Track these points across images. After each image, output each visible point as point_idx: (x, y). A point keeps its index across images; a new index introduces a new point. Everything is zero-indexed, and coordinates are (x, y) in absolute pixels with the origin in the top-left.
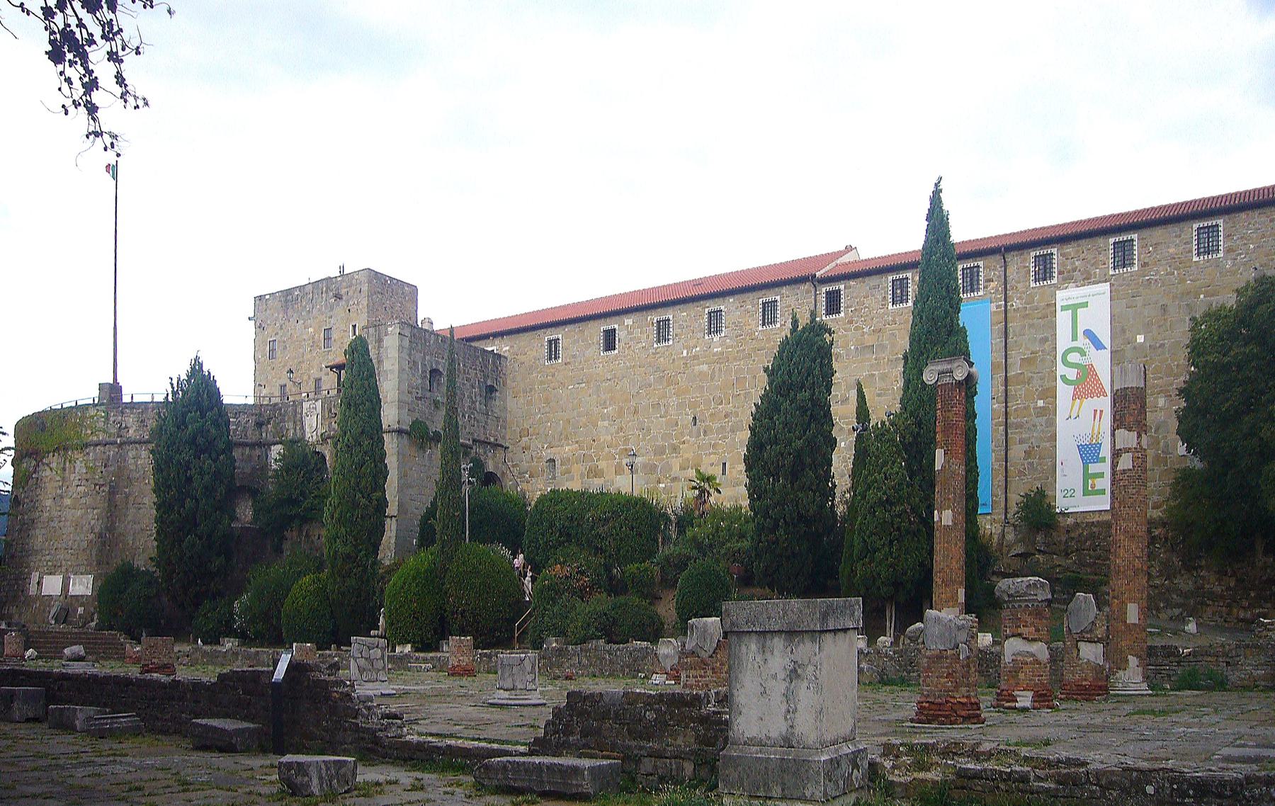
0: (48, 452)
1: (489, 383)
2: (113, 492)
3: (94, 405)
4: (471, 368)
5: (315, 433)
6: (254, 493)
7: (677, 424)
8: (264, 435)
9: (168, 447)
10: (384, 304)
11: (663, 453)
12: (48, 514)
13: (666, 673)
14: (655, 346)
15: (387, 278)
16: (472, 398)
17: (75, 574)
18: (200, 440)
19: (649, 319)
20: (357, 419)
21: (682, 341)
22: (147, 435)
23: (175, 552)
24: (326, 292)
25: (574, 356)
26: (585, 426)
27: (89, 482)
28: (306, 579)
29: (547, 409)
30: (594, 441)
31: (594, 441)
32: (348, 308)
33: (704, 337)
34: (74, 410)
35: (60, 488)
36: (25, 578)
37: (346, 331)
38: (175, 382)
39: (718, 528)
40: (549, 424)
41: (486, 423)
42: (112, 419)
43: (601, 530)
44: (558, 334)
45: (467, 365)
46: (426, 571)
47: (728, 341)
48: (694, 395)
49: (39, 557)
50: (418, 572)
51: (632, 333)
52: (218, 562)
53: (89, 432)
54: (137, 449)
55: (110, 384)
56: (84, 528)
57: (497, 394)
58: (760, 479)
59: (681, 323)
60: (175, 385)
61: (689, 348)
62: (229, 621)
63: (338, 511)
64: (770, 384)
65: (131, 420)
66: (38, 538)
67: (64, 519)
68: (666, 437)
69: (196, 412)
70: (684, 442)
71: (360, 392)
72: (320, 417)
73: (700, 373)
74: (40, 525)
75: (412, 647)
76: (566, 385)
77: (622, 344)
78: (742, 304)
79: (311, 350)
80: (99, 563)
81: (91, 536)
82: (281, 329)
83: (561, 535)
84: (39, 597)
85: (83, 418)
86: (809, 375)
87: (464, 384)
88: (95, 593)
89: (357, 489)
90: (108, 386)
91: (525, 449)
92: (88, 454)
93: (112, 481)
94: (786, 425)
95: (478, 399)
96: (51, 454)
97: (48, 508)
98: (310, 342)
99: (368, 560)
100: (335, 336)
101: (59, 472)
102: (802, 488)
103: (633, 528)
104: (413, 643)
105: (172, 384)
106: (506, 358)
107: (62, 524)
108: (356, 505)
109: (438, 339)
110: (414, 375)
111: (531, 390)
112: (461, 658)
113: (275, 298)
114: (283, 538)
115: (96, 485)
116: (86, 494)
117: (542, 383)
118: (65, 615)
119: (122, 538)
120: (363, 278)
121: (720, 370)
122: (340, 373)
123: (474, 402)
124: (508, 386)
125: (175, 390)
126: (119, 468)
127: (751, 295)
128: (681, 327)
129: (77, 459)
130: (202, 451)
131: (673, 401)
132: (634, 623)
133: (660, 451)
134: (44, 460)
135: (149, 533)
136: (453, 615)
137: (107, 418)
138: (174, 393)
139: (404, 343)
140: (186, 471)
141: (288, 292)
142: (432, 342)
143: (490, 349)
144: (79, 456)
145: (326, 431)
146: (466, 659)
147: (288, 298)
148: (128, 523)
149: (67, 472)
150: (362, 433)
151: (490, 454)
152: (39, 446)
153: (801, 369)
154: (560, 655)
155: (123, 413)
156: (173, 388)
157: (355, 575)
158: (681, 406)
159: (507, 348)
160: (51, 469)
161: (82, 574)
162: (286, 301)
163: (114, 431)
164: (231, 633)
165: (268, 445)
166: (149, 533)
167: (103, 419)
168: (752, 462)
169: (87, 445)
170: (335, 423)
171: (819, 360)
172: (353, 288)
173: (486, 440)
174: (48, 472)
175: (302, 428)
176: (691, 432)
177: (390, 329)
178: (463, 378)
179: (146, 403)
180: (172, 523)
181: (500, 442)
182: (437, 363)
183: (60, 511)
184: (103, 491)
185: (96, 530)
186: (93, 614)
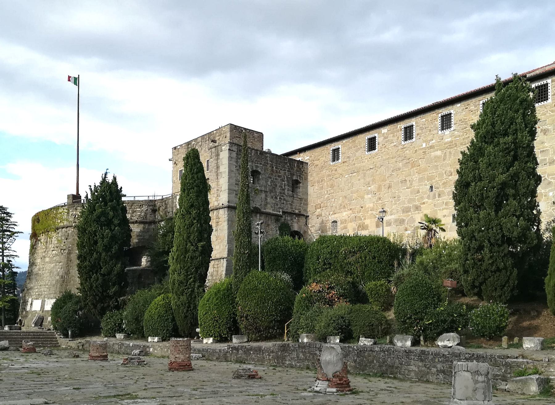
1: (295, 178)
4: (281, 169)
7: (418, 192)
11: (409, 211)
13: (328, 380)
14: (403, 143)
15: (243, 129)
16: (282, 187)
17: (48, 299)
19: (398, 127)
21: (422, 137)
25: (349, 157)
26: (356, 199)
28: (159, 298)
29: (332, 191)
30: (362, 207)
31: (362, 207)
34: (52, 210)
35: (45, 252)
38: (93, 188)
39: (440, 255)
40: (333, 200)
41: (292, 202)
42: (71, 213)
46: (224, 290)
47: (456, 133)
50: (219, 291)
51: (387, 138)
53: (59, 221)
57: (301, 185)
58: (466, 210)
59: (421, 126)
61: (427, 142)
64: (476, 136)
70: (424, 203)
71: (191, 181)
75: (213, 340)
76: (344, 175)
77: (381, 145)
78: (467, 107)
83: (325, 264)
84: (31, 312)
86: (512, 124)
87: (276, 179)
91: (318, 216)
92: (58, 233)
93: (69, 247)
94: (490, 165)
95: (287, 187)
99: (194, 285)
102: (505, 216)
103: (375, 258)
105: (91, 189)
106: (307, 164)
107: (44, 271)
109: (257, 153)
111: (322, 181)
112: (177, 356)
115: (61, 250)
116: (56, 255)
117: (329, 175)
119: (73, 278)
120: (228, 129)
121: (450, 153)
123: (284, 190)
127: (474, 100)
128: (422, 129)
131: (416, 177)
132: (364, 324)
133: (406, 210)
136: (241, 318)
137: (68, 213)
138: (93, 194)
139: (232, 156)
142: (253, 154)
143: (298, 159)
144: (54, 234)
146: (182, 357)
151: (295, 220)
153: (504, 120)
154: (283, 350)
155: (76, 209)
157: (186, 294)
158: (421, 180)
159: (308, 158)
164: (121, 330)
168: (458, 198)
171: (521, 111)
172: (222, 136)
173: (292, 212)
176: (429, 196)
177: (223, 148)
178: (276, 175)
180: (86, 267)
181: (302, 212)
182: (257, 167)
184: (65, 253)
185: (60, 274)
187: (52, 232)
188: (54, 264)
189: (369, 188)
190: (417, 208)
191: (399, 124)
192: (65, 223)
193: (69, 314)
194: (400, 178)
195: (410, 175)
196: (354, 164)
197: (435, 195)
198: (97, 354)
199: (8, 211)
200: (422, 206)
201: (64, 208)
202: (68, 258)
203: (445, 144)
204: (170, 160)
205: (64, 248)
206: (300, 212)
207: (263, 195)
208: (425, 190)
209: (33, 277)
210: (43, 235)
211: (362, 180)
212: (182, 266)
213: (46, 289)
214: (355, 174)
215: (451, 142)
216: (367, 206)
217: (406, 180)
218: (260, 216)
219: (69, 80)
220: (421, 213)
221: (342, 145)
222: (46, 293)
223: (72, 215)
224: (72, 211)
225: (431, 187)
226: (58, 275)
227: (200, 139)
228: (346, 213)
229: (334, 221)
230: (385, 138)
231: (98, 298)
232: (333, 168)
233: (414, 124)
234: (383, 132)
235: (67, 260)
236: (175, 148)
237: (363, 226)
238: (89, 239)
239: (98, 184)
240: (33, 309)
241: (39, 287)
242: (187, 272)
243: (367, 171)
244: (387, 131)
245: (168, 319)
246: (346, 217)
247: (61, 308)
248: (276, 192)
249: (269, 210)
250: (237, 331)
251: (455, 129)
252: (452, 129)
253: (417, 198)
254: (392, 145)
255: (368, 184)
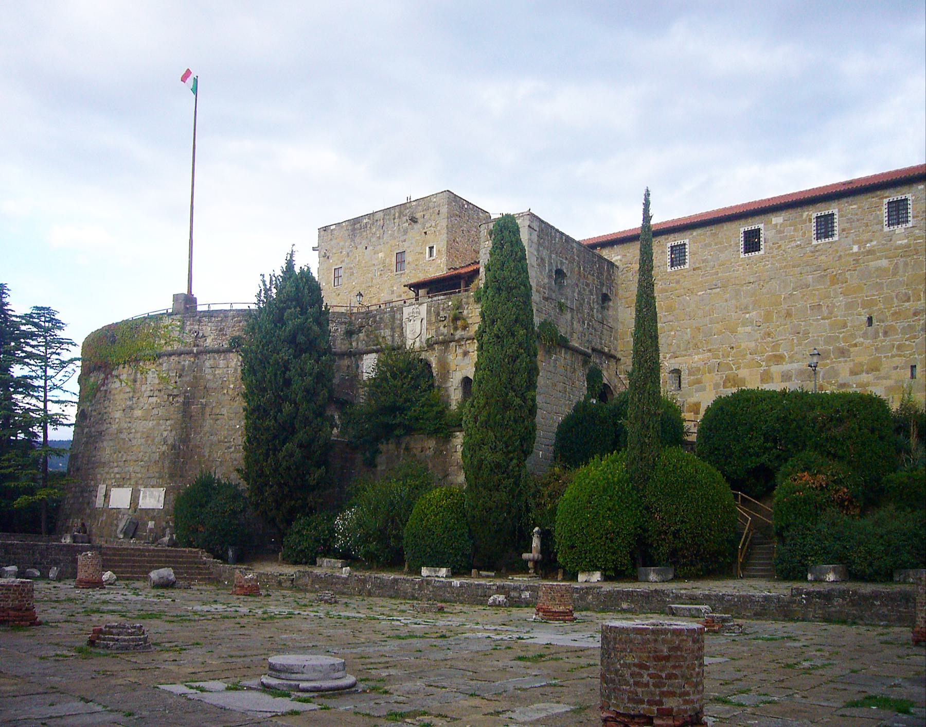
0: (119, 364)
1: (604, 291)
2: (187, 404)
3: (170, 315)
5: (418, 339)
6: (342, 404)
7: (845, 326)
8: (354, 344)
9: (263, 346)
10: (461, 227)
12: (117, 426)
18: (301, 339)
20: (510, 304)
22: (226, 344)
23: (269, 462)
24: (399, 217)
27: (163, 393)
29: (670, 318)
31: (732, 348)
32: (425, 231)
33: (882, 230)
34: (148, 321)
35: (131, 399)
36: (93, 491)
37: (422, 253)
42: (188, 328)
43: (835, 432)
44: (685, 239)
45: (586, 269)
48: (868, 294)
49: (106, 469)
52: (316, 474)
53: (163, 342)
54: (215, 359)
55: (70, 441)
56: (156, 440)
57: (611, 304)
60: (268, 283)
61: (861, 243)
62: (328, 540)
63: (485, 413)
65: (208, 329)
66: (107, 451)
67: (134, 431)
68: (829, 340)
69: (295, 308)
70: (855, 345)
72: (425, 322)
73: (877, 269)
74: (107, 437)
77: (770, 244)
79: (381, 274)
80: (172, 476)
81: (164, 448)
82: (348, 256)
83: (766, 440)
84: (107, 510)
85: (157, 328)
88: (170, 507)
89: (509, 386)
90: (183, 296)
92: (161, 364)
93: (186, 391)
96: (122, 366)
97: (117, 420)
98: (381, 267)
100: (409, 258)
101: (129, 384)
104: (604, 571)
105: (264, 282)
107: (131, 436)
108: (506, 406)
110: (541, 273)
113: (342, 227)
114: (377, 451)
116: (158, 405)
118: (133, 530)
120: (443, 200)
122: (418, 291)
123: (592, 309)
124: (620, 296)
125: (268, 287)
126: (195, 377)
128: (850, 221)
129: (150, 370)
130: (303, 351)
134: (113, 373)
135: (228, 444)
137: (183, 328)
140: (284, 373)
141: (356, 221)
142: (557, 239)
145: (433, 337)
147: (356, 226)
148: (205, 434)
149: (138, 383)
150: (516, 321)
152: (109, 358)
156: (265, 285)
158: (849, 306)
159: (619, 257)
160: (121, 381)
161: (153, 487)
162: (354, 230)
163: (189, 340)
164: (329, 552)
165: (358, 355)
166: (228, 444)
167: (179, 329)
169: (160, 356)
170: (445, 327)
174: (117, 384)
175: (402, 334)
179: (225, 310)
181: (613, 352)
182: (562, 263)
183: (130, 422)
184: (177, 402)
185: (169, 442)
186: (165, 529)
187: (148, 363)
188: (155, 422)
189: (747, 316)
190: (843, 353)
191: (805, 210)
192: (176, 346)
193: (224, 517)
194: (810, 301)
195: (829, 297)
196: (717, 273)
197: (877, 333)
198: (561, 608)
199: (57, 317)
200: (852, 349)
201: (174, 317)
202: (185, 411)
203: (896, 249)
204: (314, 249)
205: (176, 392)
206: (610, 350)
207: (569, 316)
208: (857, 323)
209: (105, 443)
210: (124, 368)
211: (734, 302)
212: (498, 435)
213: (138, 469)
214: (719, 289)
215: (908, 246)
216: (743, 346)
217: (819, 305)
218: (566, 353)
219: (184, 78)
220: (850, 361)
221: (690, 239)
222: (139, 475)
223: (190, 331)
224: (191, 324)
225: (870, 320)
226: (165, 442)
227: (381, 214)
228: (700, 356)
229: (675, 370)
230: (780, 232)
231: (286, 490)
232: (672, 278)
233: (835, 211)
234: (773, 223)
235: (184, 416)
236: (325, 229)
237: (734, 380)
238: (276, 375)
239: (279, 273)
240: (113, 504)
241: (121, 464)
242: (507, 447)
243: (742, 286)
244: (782, 221)
245: (463, 534)
246: (700, 365)
247: (202, 506)
248: (582, 313)
249: (575, 344)
250: (649, 562)
251: (914, 225)
252: (910, 225)
253: (841, 336)
254: (793, 244)
255: (746, 310)
